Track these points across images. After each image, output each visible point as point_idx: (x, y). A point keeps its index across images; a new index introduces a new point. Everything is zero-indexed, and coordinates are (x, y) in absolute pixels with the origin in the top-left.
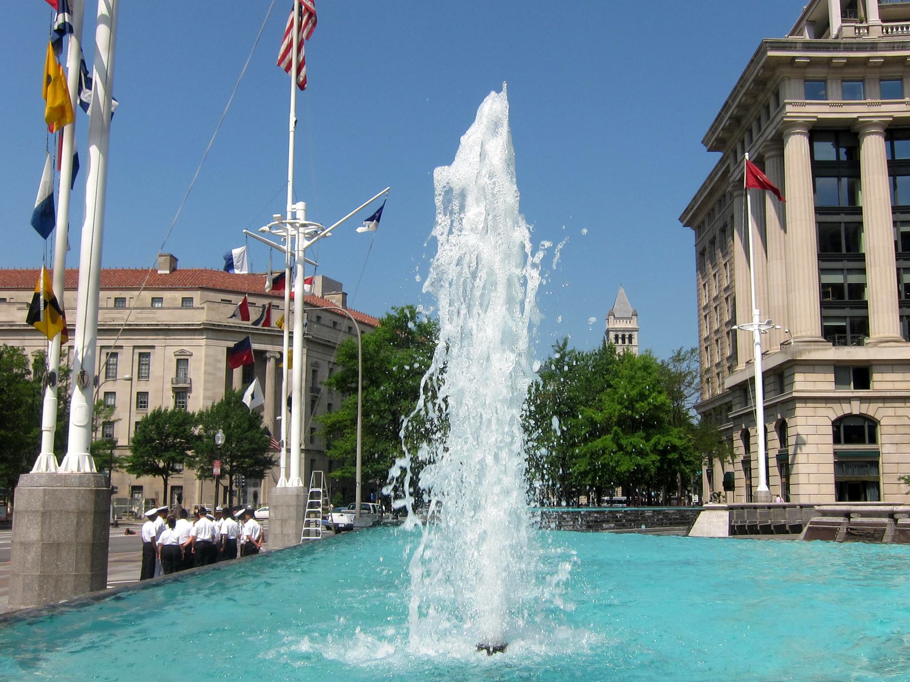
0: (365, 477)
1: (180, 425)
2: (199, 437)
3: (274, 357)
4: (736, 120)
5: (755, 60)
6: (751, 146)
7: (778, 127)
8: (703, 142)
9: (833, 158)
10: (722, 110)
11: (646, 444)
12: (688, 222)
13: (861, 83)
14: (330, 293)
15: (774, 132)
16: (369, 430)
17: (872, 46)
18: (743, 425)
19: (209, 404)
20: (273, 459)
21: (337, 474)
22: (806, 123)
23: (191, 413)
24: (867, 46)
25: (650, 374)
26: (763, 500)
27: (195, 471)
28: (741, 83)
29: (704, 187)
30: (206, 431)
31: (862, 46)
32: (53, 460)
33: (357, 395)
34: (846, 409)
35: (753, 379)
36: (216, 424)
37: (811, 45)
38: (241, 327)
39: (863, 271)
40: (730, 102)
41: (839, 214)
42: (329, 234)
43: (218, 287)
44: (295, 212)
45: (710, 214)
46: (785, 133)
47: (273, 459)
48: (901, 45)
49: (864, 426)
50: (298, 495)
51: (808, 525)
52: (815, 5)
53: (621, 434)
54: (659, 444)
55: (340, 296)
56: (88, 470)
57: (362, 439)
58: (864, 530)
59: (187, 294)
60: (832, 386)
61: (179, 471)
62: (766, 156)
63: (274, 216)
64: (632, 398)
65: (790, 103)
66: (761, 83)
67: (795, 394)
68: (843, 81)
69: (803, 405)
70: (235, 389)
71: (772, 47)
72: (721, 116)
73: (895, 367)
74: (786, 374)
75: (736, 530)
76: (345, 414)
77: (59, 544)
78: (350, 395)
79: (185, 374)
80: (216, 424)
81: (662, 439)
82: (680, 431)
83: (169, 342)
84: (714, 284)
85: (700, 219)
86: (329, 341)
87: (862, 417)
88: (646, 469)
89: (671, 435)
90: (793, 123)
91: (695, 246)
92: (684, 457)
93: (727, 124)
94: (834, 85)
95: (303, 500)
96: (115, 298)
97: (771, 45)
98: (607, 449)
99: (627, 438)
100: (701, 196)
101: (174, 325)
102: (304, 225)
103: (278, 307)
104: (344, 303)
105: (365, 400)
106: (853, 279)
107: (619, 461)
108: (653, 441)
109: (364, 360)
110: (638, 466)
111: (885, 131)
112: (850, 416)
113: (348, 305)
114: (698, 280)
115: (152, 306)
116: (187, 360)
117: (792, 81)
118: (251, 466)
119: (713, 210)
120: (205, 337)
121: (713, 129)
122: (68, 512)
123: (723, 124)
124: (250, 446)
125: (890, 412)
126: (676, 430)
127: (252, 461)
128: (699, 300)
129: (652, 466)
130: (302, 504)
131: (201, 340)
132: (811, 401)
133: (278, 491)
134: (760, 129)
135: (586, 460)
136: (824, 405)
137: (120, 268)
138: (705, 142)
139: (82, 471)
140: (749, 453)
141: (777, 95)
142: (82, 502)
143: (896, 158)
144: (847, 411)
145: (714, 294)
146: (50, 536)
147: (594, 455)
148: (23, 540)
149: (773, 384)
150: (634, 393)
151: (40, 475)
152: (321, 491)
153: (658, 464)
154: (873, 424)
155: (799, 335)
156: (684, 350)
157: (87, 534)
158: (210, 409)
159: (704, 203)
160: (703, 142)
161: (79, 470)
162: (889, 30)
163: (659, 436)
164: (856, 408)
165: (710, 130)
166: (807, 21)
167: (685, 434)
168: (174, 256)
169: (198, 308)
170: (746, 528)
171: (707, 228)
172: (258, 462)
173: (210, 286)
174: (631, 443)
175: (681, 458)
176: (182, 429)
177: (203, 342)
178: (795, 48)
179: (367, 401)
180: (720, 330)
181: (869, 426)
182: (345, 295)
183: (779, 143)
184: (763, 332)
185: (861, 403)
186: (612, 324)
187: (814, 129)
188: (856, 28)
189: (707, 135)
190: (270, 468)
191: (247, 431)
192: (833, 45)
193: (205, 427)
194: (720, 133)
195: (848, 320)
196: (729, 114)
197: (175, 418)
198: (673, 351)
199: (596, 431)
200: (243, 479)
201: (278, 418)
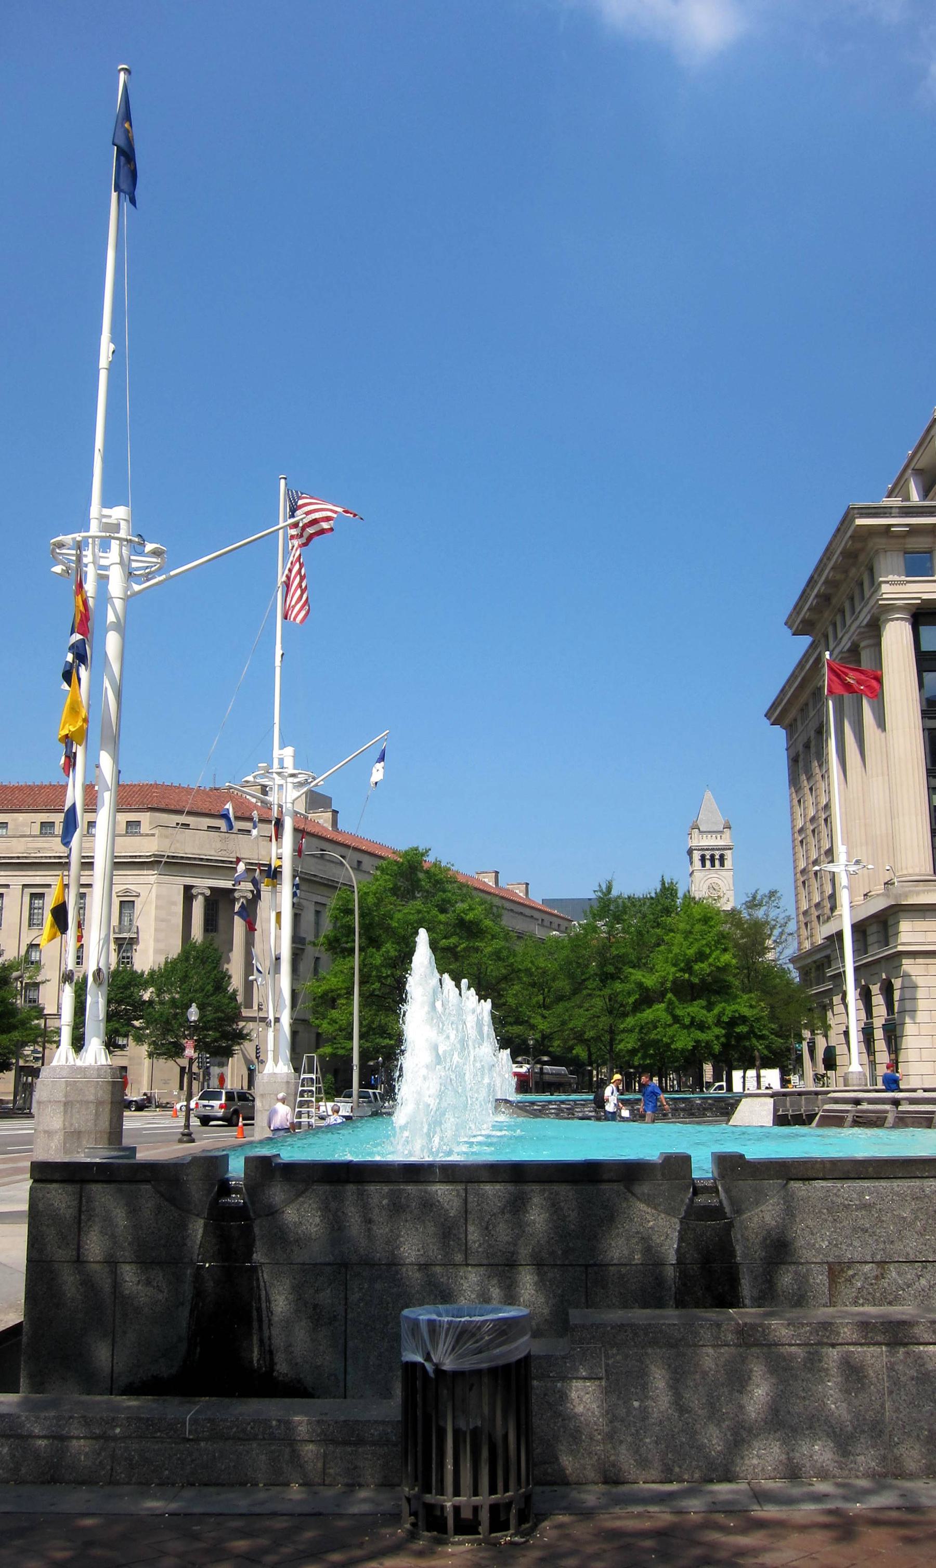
0: (365, 1055)
1: (126, 987)
2: (151, 1002)
4: (825, 599)
5: (842, 530)
6: (853, 619)
7: (872, 612)
8: (786, 624)
10: (807, 585)
11: (708, 1015)
12: (775, 720)
14: (316, 811)
15: (868, 617)
16: (368, 1000)
18: (863, 981)
19: (162, 960)
20: (245, 1032)
21: (327, 1051)
23: (139, 971)
25: (711, 927)
26: (855, 1083)
27: (146, 1047)
28: (828, 555)
29: (793, 676)
30: (158, 996)
32: (71, 1052)
33: (354, 957)
35: (840, 935)
36: (171, 986)
37: (911, 510)
38: (201, 859)
40: (816, 576)
42: (322, 783)
43: (172, 807)
44: (283, 759)
45: (804, 710)
46: (883, 618)
47: (245, 1032)
50: (288, 1082)
51: (821, 1113)
52: (923, 448)
53: (677, 1003)
54: (724, 1014)
56: (104, 1063)
57: (360, 1011)
58: (868, 1117)
59: (133, 817)
61: (122, 1047)
62: (862, 644)
63: (260, 765)
64: (688, 959)
66: (850, 556)
67: (900, 948)
70: (196, 941)
72: (806, 594)
74: (891, 922)
75: (781, 1120)
76: (338, 981)
77: (80, 1132)
78: (344, 958)
79: (131, 920)
80: (171, 986)
81: (728, 1008)
82: (751, 998)
84: (810, 799)
85: (793, 713)
86: (315, 876)
88: (708, 1044)
89: (739, 1004)
90: (891, 606)
91: (787, 749)
92: (756, 1030)
93: (814, 603)
95: (293, 1088)
96: (41, 823)
97: (860, 511)
98: (659, 1021)
99: (684, 1008)
100: (790, 687)
102: (293, 775)
104: (335, 823)
105: (363, 965)
107: (674, 1036)
108: (716, 1011)
109: (362, 916)
110: (698, 1042)
113: (340, 826)
114: (791, 795)
115: (88, 832)
116: (133, 902)
117: (889, 553)
118: (216, 1040)
119: (807, 704)
120: (156, 872)
121: (798, 608)
122: (88, 1102)
123: (809, 603)
124: (215, 1015)
126: (746, 997)
127: (218, 1034)
128: (793, 820)
129: (715, 1042)
130: (292, 1091)
131: (151, 877)
132: (921, 956)
133: (265, 1078)
134: (863, 598)
135: (635, 1036)
137: (46, 783)
138: (789, 624)
139: (99, 1064)
140: (872, 1018)
141: (871, 570)
142: (100, 1093)
145: (811, 813)
146: (72, 1125)
147: (643, 1028)
148: (46, 1129)
149: (876, 935)
150: (691, 952)
151: (61, 1067)
152: (314, 1077)
153: (723, 1040)
155: (905, 872)
157: (105, 1123)
158: (162, 967)
159: (795, 696)
160: (786, 624)
161: (96, 1063)
163: (723, 1004)
165: (795, 608)
167: (757, 1003)
169: (147, 835)
170: (804, 1117)
171: (800, 728)
172: (225, 1036)
173: (163, 806)
174: (689, 1014)
175: (752, 1031)
176: (128, 992)
177: (152, 879)
178: (891, 513)
179: (365, 965)
180: (807, 871)
182: (335, 813)
183: (875, 629)
186: (696, 840)
187: (919, 611)
189: (791, 615)
190: (239, 1044)
191: (212, 995)
193: (157, 990)
194: (806, 613)
196: (816, 591)
197: (119, 979)
198: (747, 894)
199: (647, 998)
200: (207, 1058)
201: (251, 978)
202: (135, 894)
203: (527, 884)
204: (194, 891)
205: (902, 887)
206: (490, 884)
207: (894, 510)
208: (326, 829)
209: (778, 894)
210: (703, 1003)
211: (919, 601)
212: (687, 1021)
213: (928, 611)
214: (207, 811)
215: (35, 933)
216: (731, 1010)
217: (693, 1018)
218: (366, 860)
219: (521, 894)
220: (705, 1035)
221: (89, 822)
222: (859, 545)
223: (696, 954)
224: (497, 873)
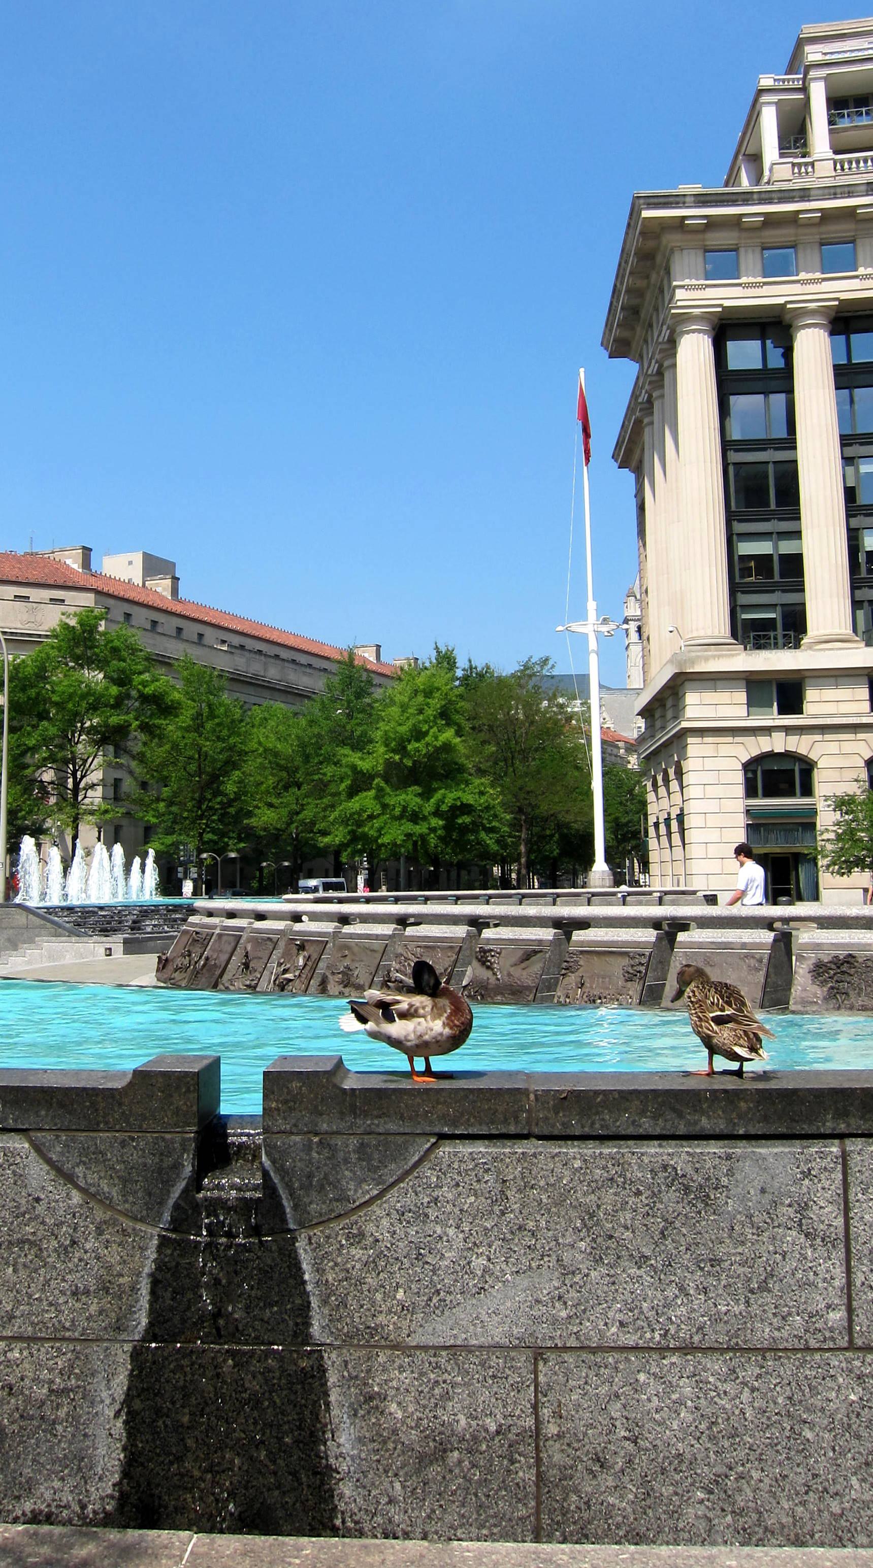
5: (632, 224)
9: (756, 364)
10: (613, 297)
13: (792, 250)
17: (802, 193)
22: (823, 309)
24: (794, 194)
31: (787, 195)
34: (764, 744)
37: (708, 198)
39: (797, 534)
40: (618, 285)
41: (765, 449)
46: (678, 329)
48: (846, 189)
49: (793, 770)
52: (749, 134)
53: (388, 790)
54: (443, 802)
55: (168, 582)
60: (743, 711)
65: (682, 287)
67: (684, 725)
68: (764, 249)
69: (698, 740)
71: (648, 204)
73: (840, 680)
87: (788, 756)
91: (635, 497)
94: (750, 256)
97: (652, 200)
99: (396, 795)
103: (63, 601)
104: (175, 591)
106: (787, 547)
107: (382, 828)
111: (830, 322)
112: (770, 756)
117: (685, 252)
125: (833, 747)
132: (710, 733)
136: (730, 739)
143: (854, 362)
144: (766, 749)
154: (808, 767)
156: (533, 660)
162: (846, 166)
164: (778, 743)
166: (744, 155)
178: (684, 203)
181: (801, 771)
184: (606, 634)
185: (786, 735)
188: (794, 165)
192: (743, 197)
195: (779, 608)
205: (690, 651)
206: (371, 659)
207: (688, 199)
208: (162, 598)
209: (551, 663)
210: (417, 789)
211: (720, 309)
212: (398, 811)
213: (737, 321)
214: (14, 579)
216: (448, 796)
217: (405, 809)
218: (208, 632)
220: (418, 827)
222: (651, 244)
223: (410, 730)
224: (378, 647)
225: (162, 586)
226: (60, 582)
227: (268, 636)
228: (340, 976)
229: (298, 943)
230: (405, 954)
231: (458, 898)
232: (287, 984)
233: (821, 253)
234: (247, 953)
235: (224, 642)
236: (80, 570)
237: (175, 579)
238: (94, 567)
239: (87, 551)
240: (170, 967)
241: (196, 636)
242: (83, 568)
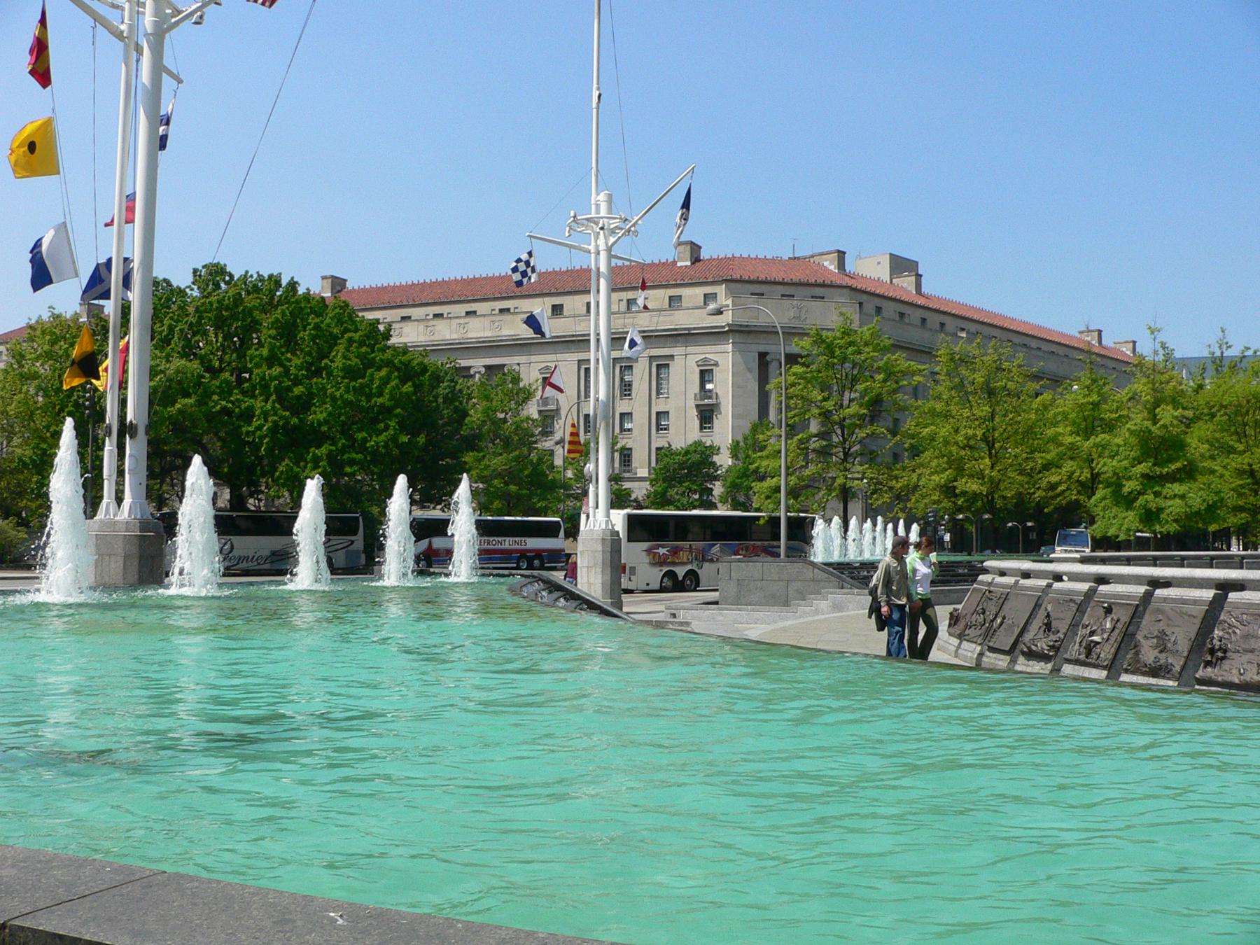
3: (479, 372)
55: (913, 278)
83: (690, 349)
101: (694, 329)
113: (924, 289)
116: (712, 370)
168: (696, 243)
202: (712, 362)
203: (1134, 342)
204: (768, 358)
208: (908, 293)
215: (625, 402)
219: (1128, 353)
221: (670, 297)
225: (906, 283)
226: (820, 281)
227: (1000, 323)
228: (1155, 640)
229: (1106, 605)
230: (1228, 621)
231: (1155, 559)
232: (1094, 646)
233: (866, 258)
234: (1048, 613)
235: (963, 330)
236: (837, 271)
237: (919, 276)
238: (848, 268)
239: (841, 254)
240: (962, 624)
241: (938, 325)
242: (839, 269)
